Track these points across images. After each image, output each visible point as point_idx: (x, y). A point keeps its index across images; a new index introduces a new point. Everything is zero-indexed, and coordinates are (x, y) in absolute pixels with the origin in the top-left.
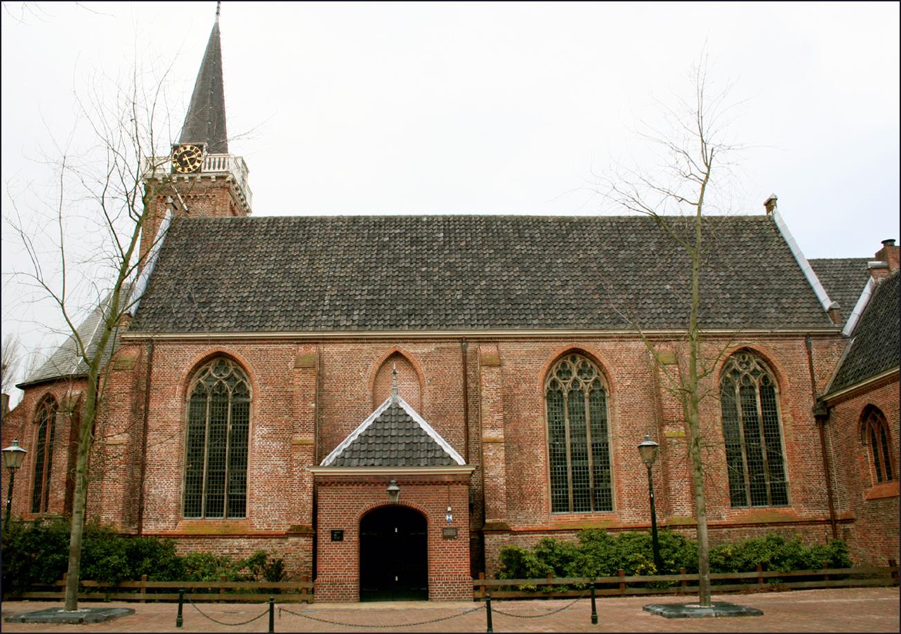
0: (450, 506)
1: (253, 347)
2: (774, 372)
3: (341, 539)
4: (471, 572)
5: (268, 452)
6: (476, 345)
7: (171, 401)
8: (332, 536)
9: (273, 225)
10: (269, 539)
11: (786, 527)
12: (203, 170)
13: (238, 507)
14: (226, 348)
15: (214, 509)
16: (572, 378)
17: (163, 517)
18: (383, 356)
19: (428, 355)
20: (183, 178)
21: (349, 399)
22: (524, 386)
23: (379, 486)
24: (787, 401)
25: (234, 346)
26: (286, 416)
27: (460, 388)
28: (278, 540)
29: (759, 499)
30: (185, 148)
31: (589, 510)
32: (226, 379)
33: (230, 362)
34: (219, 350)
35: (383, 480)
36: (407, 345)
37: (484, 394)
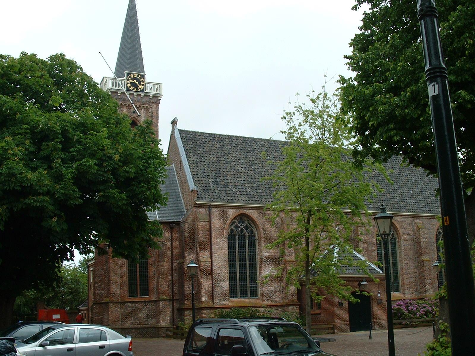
1: (259, 212)
4: (387, 318)
7: (222, 238)
12: (145, 91)
13: (254, 293)
14: (247, 212)
15: (244, 294)
17: (223, 299)
20: (140, 95)
23: (354, 282)
25: (250, 211)
28: (276, 308)
30: (134, 76)
32: (244, 227)
33: (246, 219)
34: (243, 212)
35: (356, 280)
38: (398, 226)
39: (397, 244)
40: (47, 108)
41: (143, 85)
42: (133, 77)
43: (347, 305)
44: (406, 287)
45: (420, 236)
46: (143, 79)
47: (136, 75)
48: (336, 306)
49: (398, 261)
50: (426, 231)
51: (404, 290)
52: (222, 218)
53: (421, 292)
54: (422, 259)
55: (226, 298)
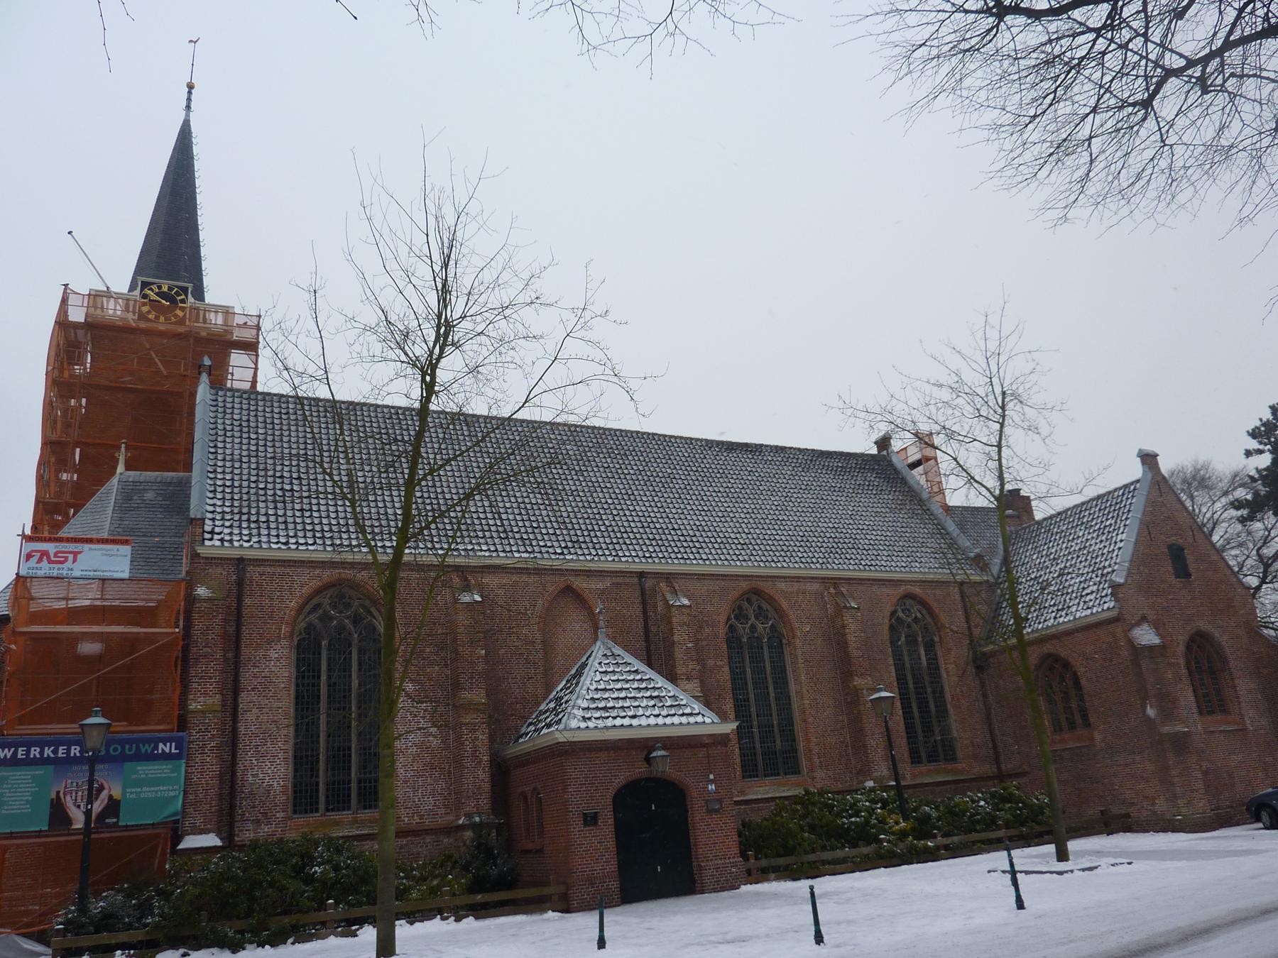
0: (711, 773)
2: (934, 619)
3: (595, 823)
5: (416, 716)
6: (654, 581)
8: (585, 820)
9: (266, 395)
10: (422, 837)
11: (961, 785)
13: (370, 796)
15: (339, 800)
16: (750, 623)
18: (554, 590)
19: (603, 592)
21: (516, 644)
22: (707, 630)
24: (949, 650)
26: (437, 668)
27: (641, 632)
29: (933, 757)
30: (160, 287)
31: (778, 775)
36: (579, 578)
37: (676, 638)
38: (784, 604)
39: (787, 650)
40: (1080, 703)
41: (183, 309)
42: (157, 290)
43: (611, 821)
44: (816, 760)
45: (844, 627)
46: (183, 297)
47: (167, 287)
48: (577, 828)
49: (793, 694)
50: (859, 614)
51: (812, 770)
52: (278, 594)
53: (858, 773)
54: (854, 686)
55: (278, 815)
